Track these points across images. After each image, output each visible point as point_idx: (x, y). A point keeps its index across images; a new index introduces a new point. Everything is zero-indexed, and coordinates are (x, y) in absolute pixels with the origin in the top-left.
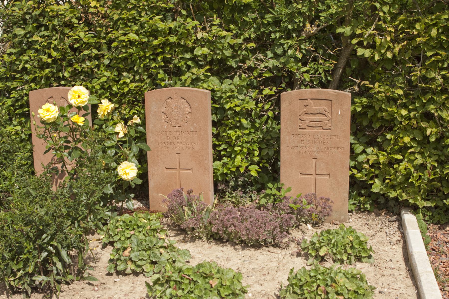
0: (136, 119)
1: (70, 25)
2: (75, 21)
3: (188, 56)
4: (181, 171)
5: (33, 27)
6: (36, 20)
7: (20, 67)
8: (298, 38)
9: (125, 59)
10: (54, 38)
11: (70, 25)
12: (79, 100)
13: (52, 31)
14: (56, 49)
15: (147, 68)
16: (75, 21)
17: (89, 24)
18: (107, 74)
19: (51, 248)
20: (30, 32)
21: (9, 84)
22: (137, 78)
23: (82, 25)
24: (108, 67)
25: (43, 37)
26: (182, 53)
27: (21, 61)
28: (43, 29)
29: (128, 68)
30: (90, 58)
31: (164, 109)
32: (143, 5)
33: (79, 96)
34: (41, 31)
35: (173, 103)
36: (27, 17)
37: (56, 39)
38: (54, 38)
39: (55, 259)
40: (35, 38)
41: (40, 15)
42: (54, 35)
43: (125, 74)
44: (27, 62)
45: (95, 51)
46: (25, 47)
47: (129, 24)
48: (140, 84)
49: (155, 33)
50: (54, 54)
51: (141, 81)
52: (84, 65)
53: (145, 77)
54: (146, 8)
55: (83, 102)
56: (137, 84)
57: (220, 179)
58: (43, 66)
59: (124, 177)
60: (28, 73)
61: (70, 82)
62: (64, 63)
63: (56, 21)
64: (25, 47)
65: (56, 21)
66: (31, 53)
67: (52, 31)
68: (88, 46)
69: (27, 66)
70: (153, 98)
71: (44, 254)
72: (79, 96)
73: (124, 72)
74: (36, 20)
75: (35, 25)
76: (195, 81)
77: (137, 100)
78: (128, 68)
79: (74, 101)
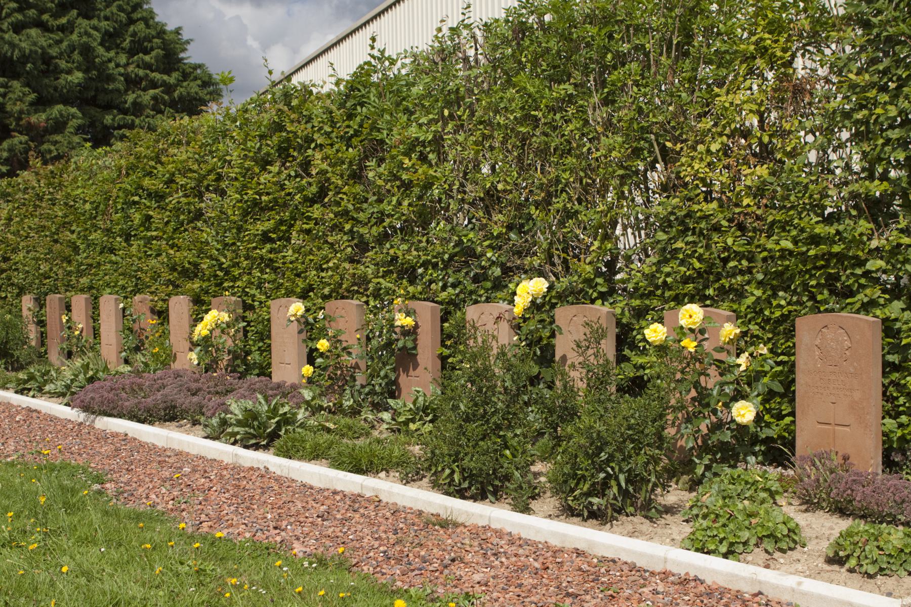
0: (762, 349)
1: (717, 228)
2: (724, 223)
3: (859, 271)
4: (837, 428)
5: (677, 230)
6: (682, 223)
7: (661, 280)
8: (623, 256)
9: (781, 274)
10: (700, 245)
11: (717, 228)
12: (690, 320)
13: (699, 236)
14: (700, 259)
15: (805, 286)
16: (724, 223)
17: (741, 227)
18: (758, 293)
19: (609, 469)
20: (674, 238)
21: (647, 302)
22: (795, 299)
23: (733, 229)
24: (760, 284)
25: (687, 244)
26: (853, 266)
27: (662, 272)
28: (690, 233)
29: (785, 285)
30: (742, 273)
31: (818, 342)
32: (804, 203)
33: (691, 317)
34: (687, 236)
35: (829, 334)
36: (672, 218)
37: (702, 247)
38: (700, 245)
39: (613, 483)
40: (679, 244)
41: (686, 216)
42: (700, 241)
43: (781, 294)
44: (668, 275)
45: (745, 263)
46: (668, 256)
47: (788, 228)
48: (798, 308)
49: (815, 240)
50: (697, 265)
51: (799, 303)
52: (733, 281)
53: (805, 299)
54: (808, 207)
55: (694, 323)
56: (795, 307)
57: (895, 446)
58: (686, 280)
59: (739, 420)
60: (670, 289)
61: (717, 302)
62: (711, 278)
63: (704, 223)
64: (668, 256)
65: (704, 223)
66: (674, 264)
67: (699, 236)
68: (739, 256)
69: (669, 280)
70: (807, 329)
71: (602, 475)
72: (691, 317)
73: (779, 291)
74: (682, 223)
75: (680, 228)
76: (868, 306)
77: (784, 328)
78: (785, 285)
79: (684, 322)
